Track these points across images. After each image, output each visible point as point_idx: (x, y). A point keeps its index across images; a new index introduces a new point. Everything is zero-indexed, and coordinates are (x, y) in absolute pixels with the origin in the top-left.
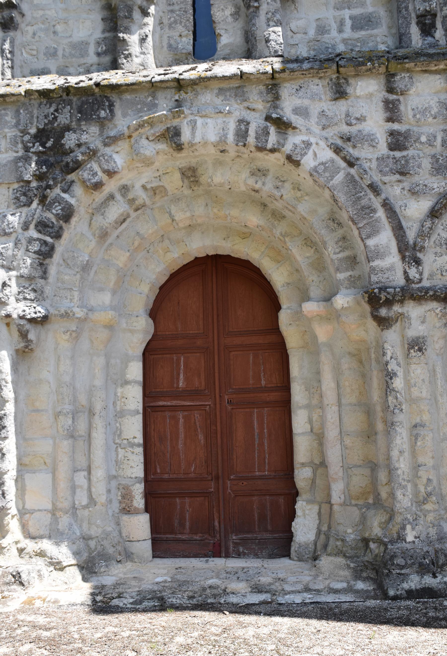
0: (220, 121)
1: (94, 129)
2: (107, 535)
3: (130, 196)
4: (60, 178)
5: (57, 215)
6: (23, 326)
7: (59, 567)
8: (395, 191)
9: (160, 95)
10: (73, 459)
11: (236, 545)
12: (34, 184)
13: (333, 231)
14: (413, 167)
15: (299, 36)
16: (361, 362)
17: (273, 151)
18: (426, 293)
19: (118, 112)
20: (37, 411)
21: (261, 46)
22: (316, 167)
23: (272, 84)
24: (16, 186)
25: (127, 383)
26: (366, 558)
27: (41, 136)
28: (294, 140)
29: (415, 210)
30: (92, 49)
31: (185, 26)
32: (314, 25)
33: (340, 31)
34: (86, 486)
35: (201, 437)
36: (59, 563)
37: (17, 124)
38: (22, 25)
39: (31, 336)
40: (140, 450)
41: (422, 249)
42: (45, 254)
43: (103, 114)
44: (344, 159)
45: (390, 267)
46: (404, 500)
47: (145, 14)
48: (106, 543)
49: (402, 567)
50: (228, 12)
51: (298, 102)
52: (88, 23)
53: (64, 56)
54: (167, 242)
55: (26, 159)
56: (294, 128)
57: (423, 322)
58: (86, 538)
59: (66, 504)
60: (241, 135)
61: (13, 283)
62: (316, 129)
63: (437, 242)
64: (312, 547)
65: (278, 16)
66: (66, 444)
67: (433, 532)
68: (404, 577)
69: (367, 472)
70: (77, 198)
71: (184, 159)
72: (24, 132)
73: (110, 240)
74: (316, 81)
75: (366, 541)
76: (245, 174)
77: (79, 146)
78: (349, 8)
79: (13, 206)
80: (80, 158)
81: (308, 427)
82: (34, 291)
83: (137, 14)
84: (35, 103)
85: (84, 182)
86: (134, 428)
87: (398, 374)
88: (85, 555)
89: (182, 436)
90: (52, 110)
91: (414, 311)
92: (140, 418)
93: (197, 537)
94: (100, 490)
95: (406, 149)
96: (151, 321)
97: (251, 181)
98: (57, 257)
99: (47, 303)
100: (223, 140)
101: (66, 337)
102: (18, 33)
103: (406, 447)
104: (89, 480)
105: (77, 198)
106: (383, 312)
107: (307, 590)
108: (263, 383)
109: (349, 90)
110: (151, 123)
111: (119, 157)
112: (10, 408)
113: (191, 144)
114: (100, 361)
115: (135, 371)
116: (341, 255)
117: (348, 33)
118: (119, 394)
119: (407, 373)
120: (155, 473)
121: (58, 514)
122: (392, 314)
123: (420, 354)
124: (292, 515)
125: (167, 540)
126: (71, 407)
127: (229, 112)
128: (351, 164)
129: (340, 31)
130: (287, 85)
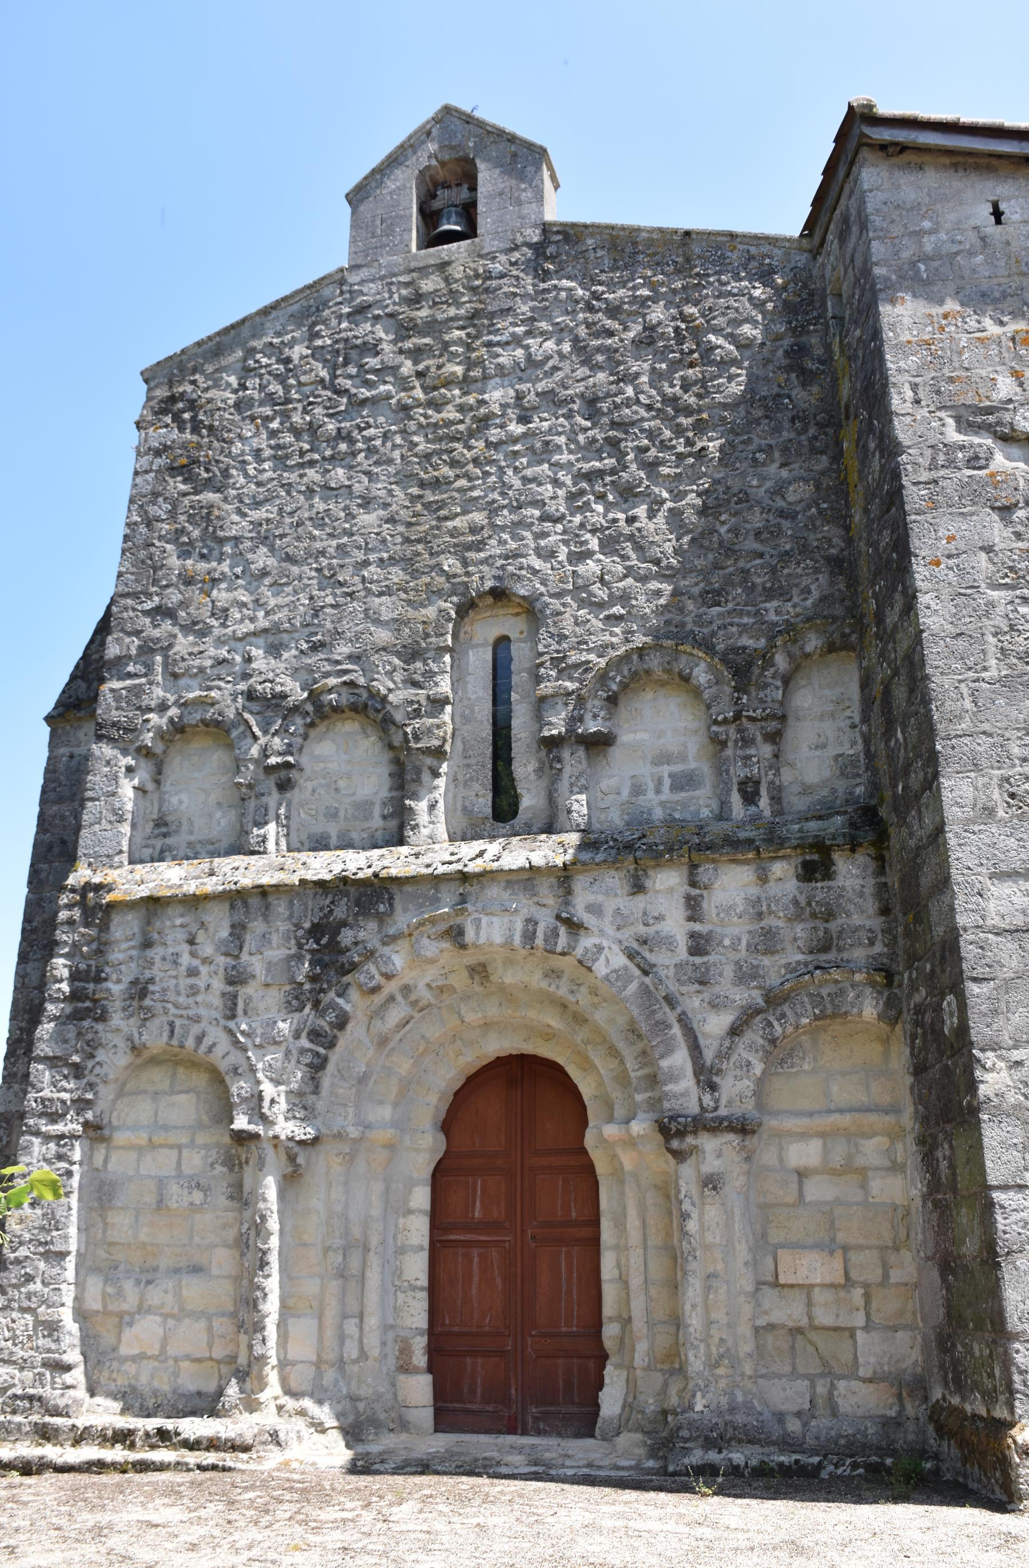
0: (506, 919)
1: (372, 925)
2: (379, 1397)
3: (413, 997)
4: (334, 980)
5: (330, 1023)
7: (320, 1428)
8: (693, 1003)
9: (443, 887)
10: (343, 1303)
11: (536, 1419)
12: (307, 986)
13: (633, 1044)
15: (611, 797)
16: (668, 1197)
17: (563, 954)
20: (304, 1245)
21: (562, 817)
23: (564, 877)
24: (288, 988)
25: (410, 1212)
27: (316, 931)
28: (586, 942)
29: (714, 1025)
30: (377, 811)
31: (482, 785)
32: (628, 784)
33: (658, 791)
35: (499, 1281)
36: (321, 1424)
37: (291, 916)
38: (301, 781)
39: (300, 1160)
40: (424, 1295)
41: (719, 1072)
42: (317, 1066)
43: (382, 908)
44: (638, 966)
45: (684, 1092)
46: (696, 1363)
47: (436, 774)
48: (377, 1406)
49: (687, 1440)
50: (531, 768)
51: (591, 898)
52: (374, 779)
54: (459, 1043)
55: (299, 958)
57: (719, 1156)
58: (354, 1399)
59: (331, 1356)
60: (529, 936)
61: (282, 1099)
62: (610, 930)
65: (583, 781)
66: (334, 1285)
67: (724, 1401)
68: (686, 1452)
69: (672, 1329)
70: (353, 1003)
71: (470, 958)
72: (298, 926)
73: (392, 1044)
74: (613, 873)
75: (665, 1413)
76: (538, 976)
77: (356, 944)
80: (356, 959)
81: (616, 1272)
82: (305, 1108)
83: (426, 776)
84: (310, 893)
85: (360, 986)
86: (417, 1268)
88: (351, 1418)
89: (476, 1279)
91: (708, 1143)
92: (425, 1255)
93: (490, 1408)
94: (373, 1341)
95: (707, 953)
96: (442, 1137)
97: (544, 984)
98: (331, 1067)
99: (318, 1122)
100: (508, 944)
101: (339, 1160)
102: (296, 790)
103: (699, 1300)
104: (361, 1329)
105: (353, 1003)
106: (675, 1144)
107: (590, 1465)
108: (574, 1215)
109: (648, 884)
110: (432, 921)
111: (398, 959)
112: (274, 1242)
113: (476, 946)
114: (378, 1187)
115: (421, 1197)
116: (639, 1073)
117: (666, 795)
119: (701, 1215)
120: (443, 1325)
121: (324, 1367)
122: (684, 1146)
124: (600, 1385)
125: (454, 1410)
126: (342, 1242)
127: (516, 910)
128: (646, 973)
129: (658, 791)
130: (580, 877)
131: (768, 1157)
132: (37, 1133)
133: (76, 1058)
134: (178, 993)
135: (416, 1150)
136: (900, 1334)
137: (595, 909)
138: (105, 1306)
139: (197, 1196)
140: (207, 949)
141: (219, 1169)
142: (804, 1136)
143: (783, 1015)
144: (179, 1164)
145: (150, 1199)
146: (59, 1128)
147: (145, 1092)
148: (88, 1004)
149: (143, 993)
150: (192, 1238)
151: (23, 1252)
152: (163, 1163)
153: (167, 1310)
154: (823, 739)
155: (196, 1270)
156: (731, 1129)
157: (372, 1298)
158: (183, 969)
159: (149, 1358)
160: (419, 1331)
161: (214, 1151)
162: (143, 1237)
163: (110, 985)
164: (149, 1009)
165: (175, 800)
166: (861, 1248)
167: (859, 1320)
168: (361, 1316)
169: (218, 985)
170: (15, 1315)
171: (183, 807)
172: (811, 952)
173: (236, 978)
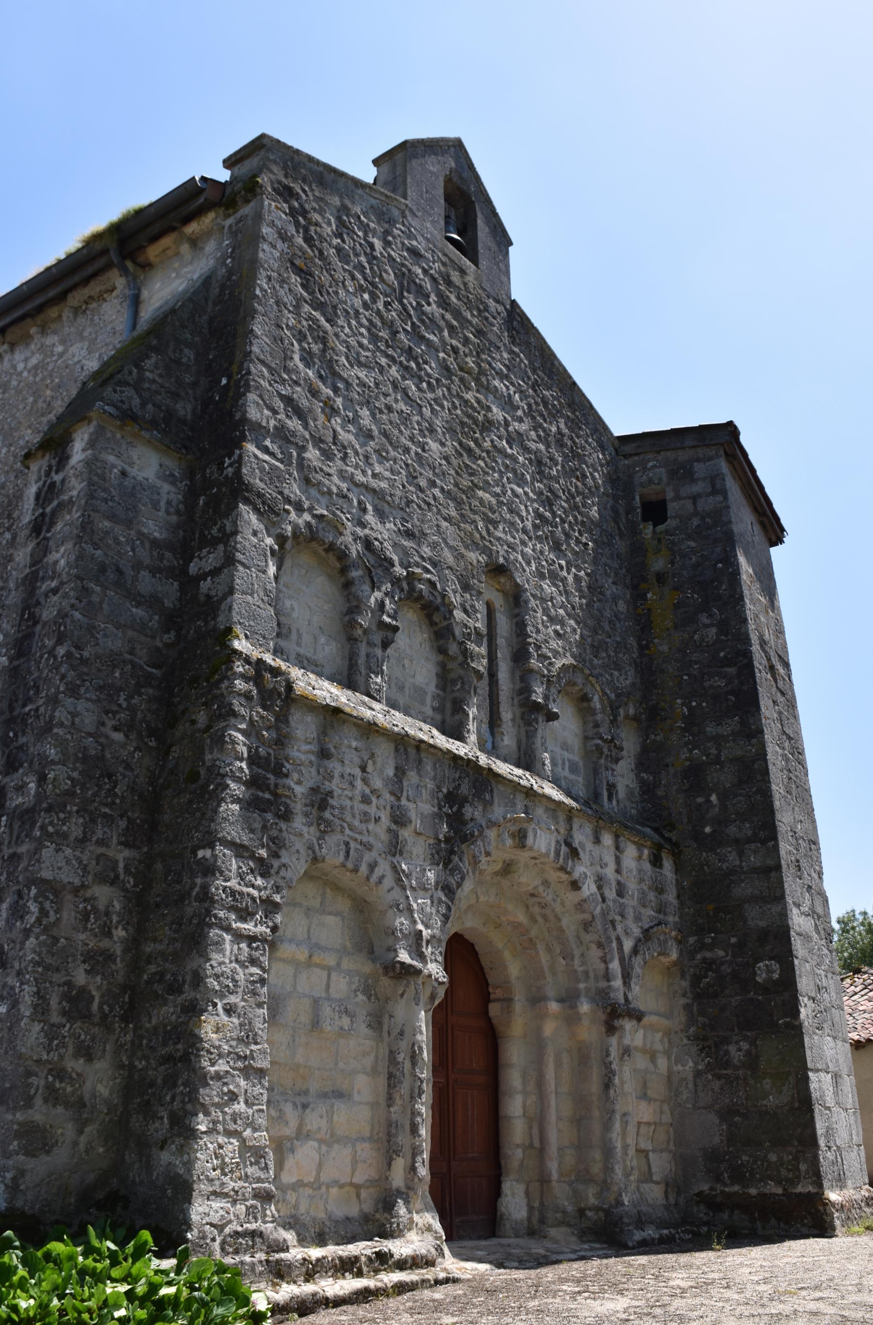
26: (583, 1226)
64: (525, 1222)
72: (439, 788)
81: (522, 1111)
132: (228, 929)
133: (263, 853)
134: (354, 816)
139: (346, 1021)
141: (361, 997)
144: (328, 986)
145: (305, 1019)
146: (248, 927)
147: (300, 905)
148: (267, 796)
149: (323, 805)
150: (337, 1064)
151: (222, 1066)
152: (312, 982)
155: (339, 1095)
159: (305, 1185)
161: (356, 979)
162: (299, 1058)
164: (329, 823)
169: (385, 820)
170: (221, 1139)
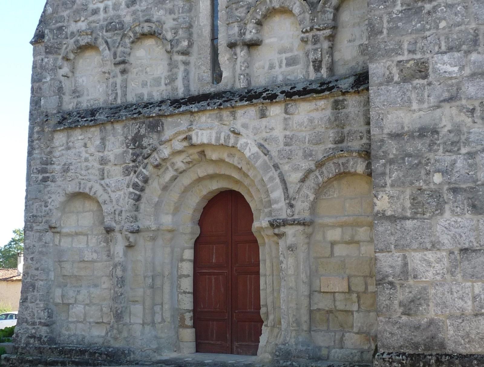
1: (155, 136)
6: (127, 235)
8: (286, 168)
14: (294, 155)
18: (294, 222)
19: (165, 128)
22: (250, 156)
29: (294, 177)
33: (280, 67)
34: (160, 313)
35: (222, 289)
50: (226, 58)
53: (150, 86)
56: (241, 135)
59: (149, 319)
63: (303, 195)
66: (149, 292)
72: (126, 138)
78: (285, 53)
79: (123, 176)
86: (187, 284)
87: (284, 262)
89: (213, 288)
90: (137, 126)
91: (290, 230)
94: (167, 315)
98: (143, 200)
102: (130, 73)
109: (267, 113)
115: (189, 254)
118: (180, 266)
123: (292, 252)
128: (266, 155)
129: (280, 67)
131: (318, 237)
135: (185, 234)
136: (371, 314)
137: (245, 126)
138: (63, 301)
140: (92, 149)
142: (334, 226)
143: (322, 173)
153: (86, 302)
154: (354, 36)
156: (299, 224)
157: (166, 297)
158: (83, 158)
160: (189, 311)
163: (55, 166)
165: (80, 80)
166: (355, 276)
167: (355, 307)
168: (162, 304)
169: (97, 165)
171: (84, 83)
172: (335, 143)
173: (103, 161)
